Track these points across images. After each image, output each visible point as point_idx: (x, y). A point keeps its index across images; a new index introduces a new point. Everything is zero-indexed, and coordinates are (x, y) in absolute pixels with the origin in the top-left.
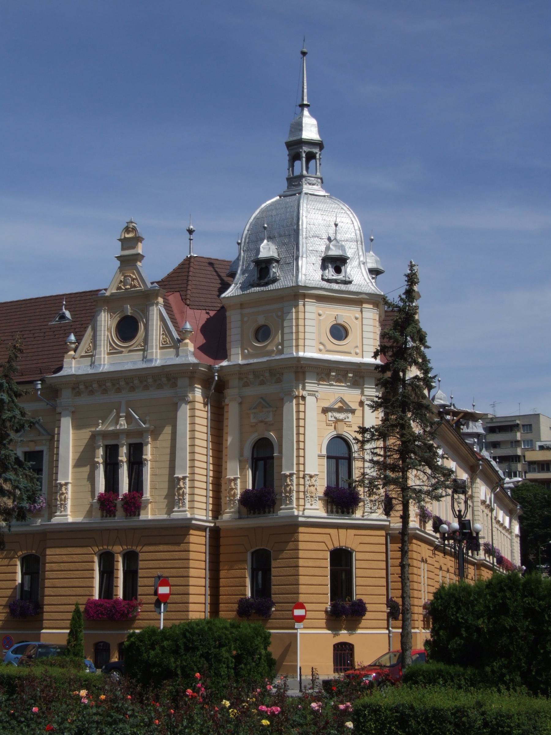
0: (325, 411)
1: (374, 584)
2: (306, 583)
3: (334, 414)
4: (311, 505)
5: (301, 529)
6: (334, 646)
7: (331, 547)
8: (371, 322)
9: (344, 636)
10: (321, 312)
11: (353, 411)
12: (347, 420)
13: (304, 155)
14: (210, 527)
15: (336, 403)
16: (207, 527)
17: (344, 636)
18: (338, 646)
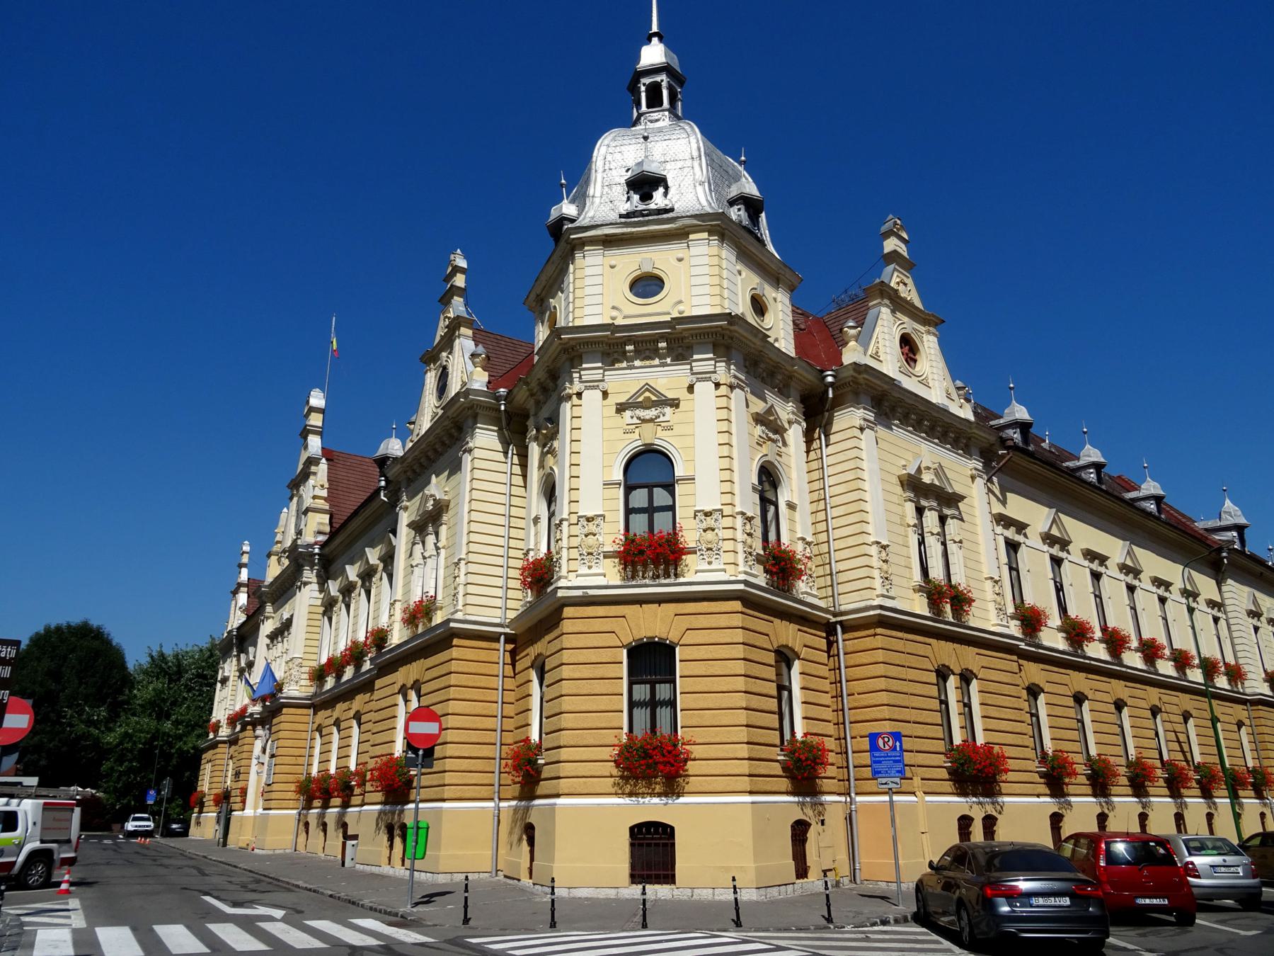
0: (621, 408)
1: (717, 706)
2: (578, 709)
3: (637, 412)
4: (590, 567)
5: (568, 612)
6: (632, 829)
7: (628, 639)
8: (931, 345)
9: (652, 808)
10: (613, 263)
11: (675, 403)
12: (662, 419)
13: (643, 88)
14: (505, 634)
15: (639, 392)
16: (501, 634)
17: (652, 808)
18: (640, 832)
